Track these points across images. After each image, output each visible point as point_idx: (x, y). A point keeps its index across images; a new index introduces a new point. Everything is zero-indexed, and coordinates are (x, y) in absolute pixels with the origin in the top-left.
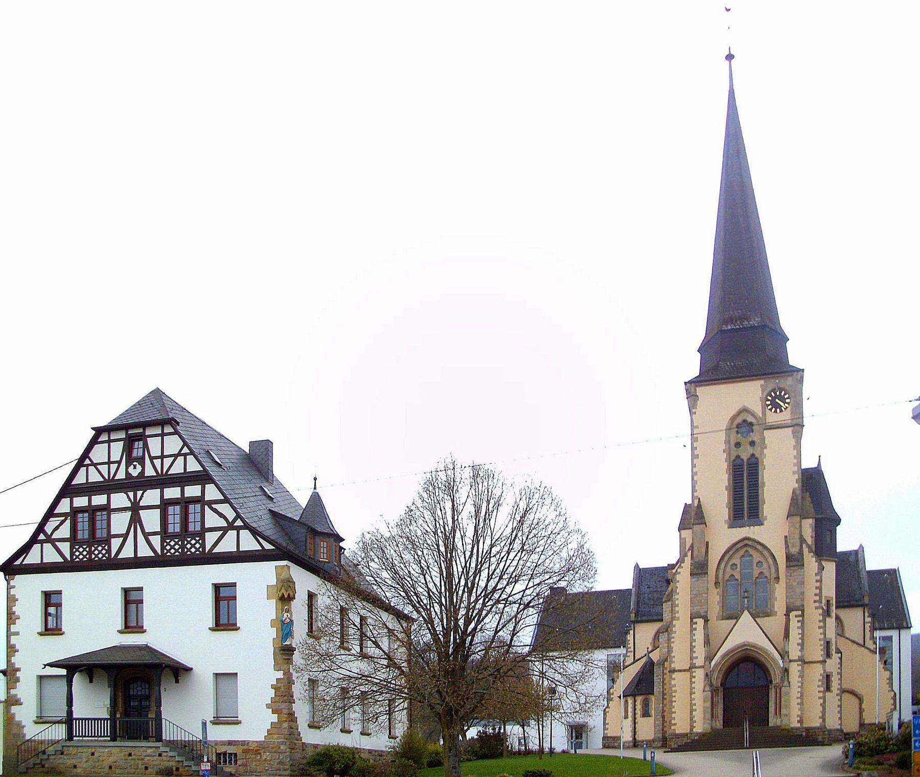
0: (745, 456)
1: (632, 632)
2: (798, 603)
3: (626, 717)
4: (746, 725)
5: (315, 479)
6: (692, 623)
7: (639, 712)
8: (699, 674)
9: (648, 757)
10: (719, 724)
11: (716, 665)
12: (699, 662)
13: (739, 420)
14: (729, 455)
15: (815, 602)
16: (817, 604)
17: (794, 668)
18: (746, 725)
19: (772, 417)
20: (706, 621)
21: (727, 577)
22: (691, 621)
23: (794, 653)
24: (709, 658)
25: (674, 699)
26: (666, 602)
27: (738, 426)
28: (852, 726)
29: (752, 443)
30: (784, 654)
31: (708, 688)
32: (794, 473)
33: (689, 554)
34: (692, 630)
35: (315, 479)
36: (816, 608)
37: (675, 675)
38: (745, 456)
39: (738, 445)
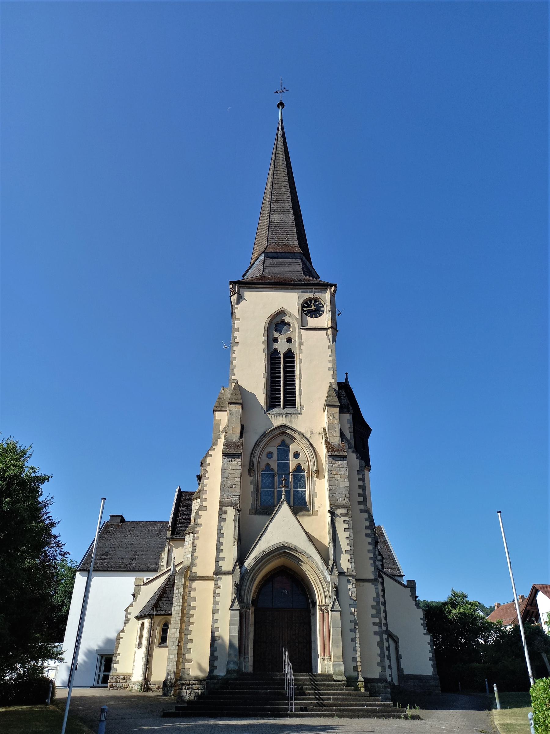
1: (166, 550)
3: (140, 647)
6: (222, 512)
7: (157, 640)
8: (227, 584)
9: (344, 511)
10: (249, 666)
12: (228, 564)
15: (359, 503)
16: (362, 507)
21: (263, 466)
22: (220, 509)
24: (241, 559)
25: (191, 620)
26: (196, 499)
28: (391, 675)
31: (236, 605)
32: (329, 369)
33: (223, 436)
34: (221, 520)
37: (195, 584)
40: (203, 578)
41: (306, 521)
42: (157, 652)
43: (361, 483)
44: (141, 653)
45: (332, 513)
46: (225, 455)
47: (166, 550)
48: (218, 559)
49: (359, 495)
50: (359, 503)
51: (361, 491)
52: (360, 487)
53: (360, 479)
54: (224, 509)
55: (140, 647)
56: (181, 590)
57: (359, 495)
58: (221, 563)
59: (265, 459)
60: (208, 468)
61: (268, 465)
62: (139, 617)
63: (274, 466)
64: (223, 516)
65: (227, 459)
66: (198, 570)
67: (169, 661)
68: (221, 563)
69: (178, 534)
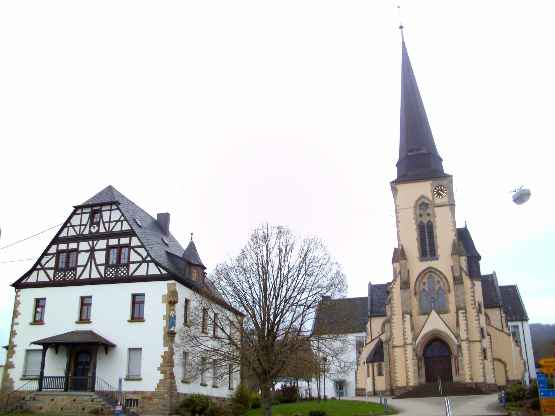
0: (425, 222)
2: (462, 305)
4: (440, 381)
5: (192, 234)
7: (376, 373)
8: (410, 349)
10: (423, 380)
11: (419, 343)
12: (409, 341)
13: (420, 202)
14: (417, 221)
15: (472, 304)
17: (464, 345)
18: (440, 381)
19: (438, 201)
20: (411, 316)
21: (421, 290)
22: (403, 316)
23: (463, 336)
24: (415, 339)
26: (387, 304)
27: (420, 205)
29: (429, 215)
30: (457, 336)
31: (415, 358)
35: (192, 234)
36: (473, 308)
38: (425, 222)
39: (421, 215)
40: (398, 347)
41: (444, 316)
42: (376, 377)
43: (472, 294)
44: (370, 379)
45: (457, 312)
46: (401, 288)
47: (369, 323)
48: (404, 339)
49: (472, 300)
50: (472, 304)
51: (473, 298)
52: (472, 296)
53: (472, 292)
54: (405, 316)
55: (368, 376)
56: (387, 350)
57: (472, 300)
58: (406, 341)
59: (422, 287)
60: (394, 294)
61: (424, 289)
62: (368, 362)
63: (427, 289)
64: (405, 319)
65: (403, 291)
66: (396, 343)
67: (386, 381)
68: (406, 341)
69: (375, 313)
